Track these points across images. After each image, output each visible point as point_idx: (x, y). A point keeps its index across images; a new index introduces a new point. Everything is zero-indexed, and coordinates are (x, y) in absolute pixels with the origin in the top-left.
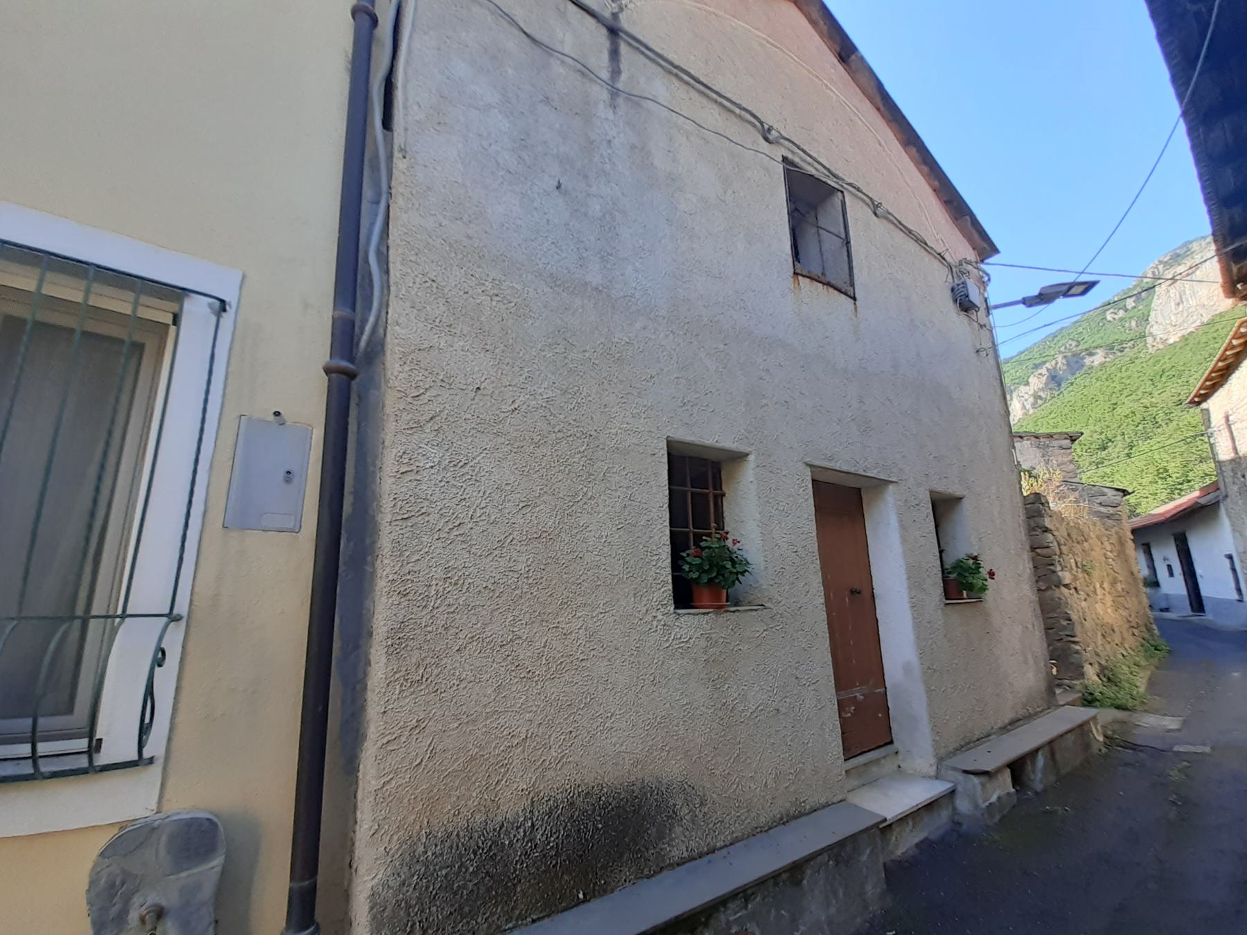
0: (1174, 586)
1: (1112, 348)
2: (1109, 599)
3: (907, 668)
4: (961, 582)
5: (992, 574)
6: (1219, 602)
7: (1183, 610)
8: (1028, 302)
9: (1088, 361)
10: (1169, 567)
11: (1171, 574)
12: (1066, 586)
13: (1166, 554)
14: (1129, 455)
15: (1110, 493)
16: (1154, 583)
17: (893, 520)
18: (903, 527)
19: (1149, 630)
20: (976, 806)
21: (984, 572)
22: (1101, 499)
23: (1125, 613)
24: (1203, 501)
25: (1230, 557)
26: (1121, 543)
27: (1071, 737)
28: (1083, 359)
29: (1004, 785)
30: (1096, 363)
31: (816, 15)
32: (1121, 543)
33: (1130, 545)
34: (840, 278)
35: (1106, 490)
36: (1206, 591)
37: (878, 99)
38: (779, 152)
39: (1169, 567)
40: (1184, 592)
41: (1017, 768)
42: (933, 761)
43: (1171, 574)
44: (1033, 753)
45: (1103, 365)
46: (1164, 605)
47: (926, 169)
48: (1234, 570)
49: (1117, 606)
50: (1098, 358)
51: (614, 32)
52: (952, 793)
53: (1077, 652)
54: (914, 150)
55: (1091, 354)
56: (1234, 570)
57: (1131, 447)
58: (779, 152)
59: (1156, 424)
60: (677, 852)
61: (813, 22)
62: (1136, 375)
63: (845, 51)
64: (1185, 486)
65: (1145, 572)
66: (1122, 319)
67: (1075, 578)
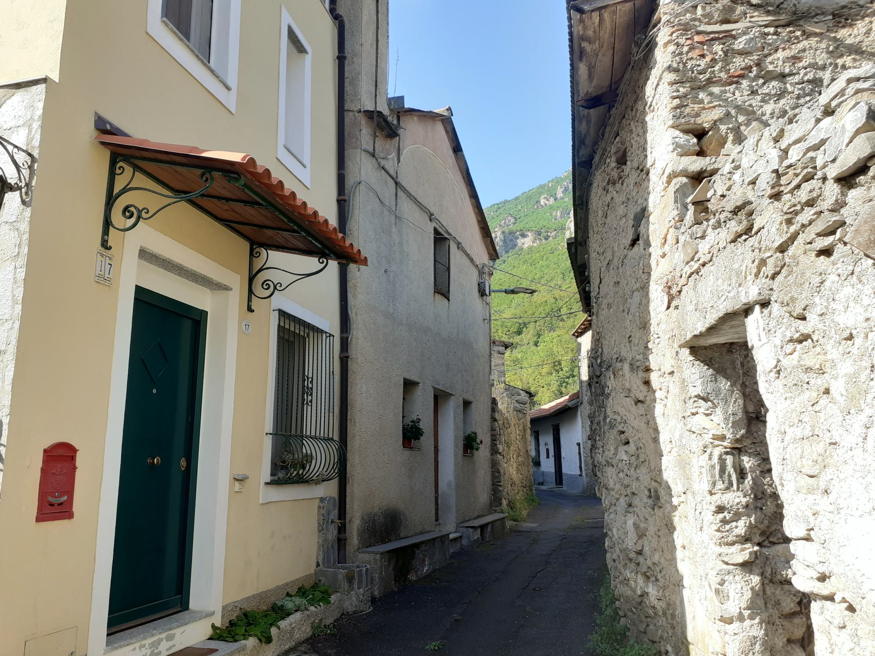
0: (548, 465)
1: (540, 234)
2: (515, 465)
3: (449, 484)
4: (469, 444)
5: (481, 442)
6: (571, 476)
7: (551, 484)
8: (506, 292)
9: (520, 241)
10: (548, 450)
11: (548, 457)
12: (500, 453)
13: (547, 440)
14: (536, 344)
15: (523, 394)
16: (537, 463)
17: (452, 416)
18: (455, 417)
19: (531, 490)
20: (470, 541)
21: (478, 441)
22: (518, 398)
23: (521, 476)
24: (570, 404)
25: (579, 444)
26: (524, 430)
27: (499, 522)
28: (517, 238)
29: (477, 535)
30: (526, 246)
31: (449, 129)
32: (524, 430)
33: (529, 432)
34: (444, 290)
35: (521, 392)
36: (565, 470)
37: (465, 173)
38: (434, 225)
39: (548, 450)
40: (552, 470)
41: (483, 527)
42: (455, 525)
43: (548, 457)
44: (488, 524)
45: (530, 248)
46: (541, 480)
47: (477, 210)
48: (580, 453)
49: (518, 470)
50: (526, 242)
51: (396, 183)
52: (461, 537)
53: (500, 491)
54: (474, 201)
55: (524, 236)
56: (580, 453)
57: (539, 336)
58: (434, 225)
59: (559, 317)
60: (402, 535)
61: (447, 131)
62: (552, 266)
63: (457, 149)
64: (571, 380)
65: (533, 453)
66: (551, 207)
67: (504, 450)
